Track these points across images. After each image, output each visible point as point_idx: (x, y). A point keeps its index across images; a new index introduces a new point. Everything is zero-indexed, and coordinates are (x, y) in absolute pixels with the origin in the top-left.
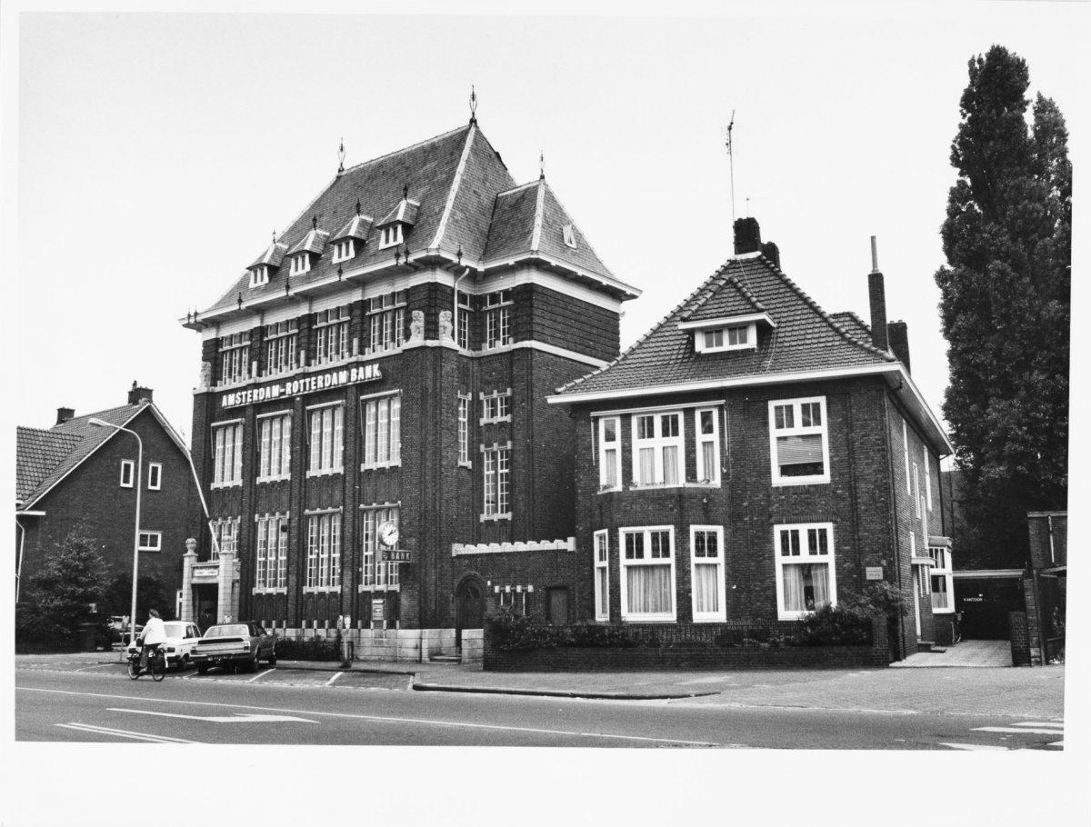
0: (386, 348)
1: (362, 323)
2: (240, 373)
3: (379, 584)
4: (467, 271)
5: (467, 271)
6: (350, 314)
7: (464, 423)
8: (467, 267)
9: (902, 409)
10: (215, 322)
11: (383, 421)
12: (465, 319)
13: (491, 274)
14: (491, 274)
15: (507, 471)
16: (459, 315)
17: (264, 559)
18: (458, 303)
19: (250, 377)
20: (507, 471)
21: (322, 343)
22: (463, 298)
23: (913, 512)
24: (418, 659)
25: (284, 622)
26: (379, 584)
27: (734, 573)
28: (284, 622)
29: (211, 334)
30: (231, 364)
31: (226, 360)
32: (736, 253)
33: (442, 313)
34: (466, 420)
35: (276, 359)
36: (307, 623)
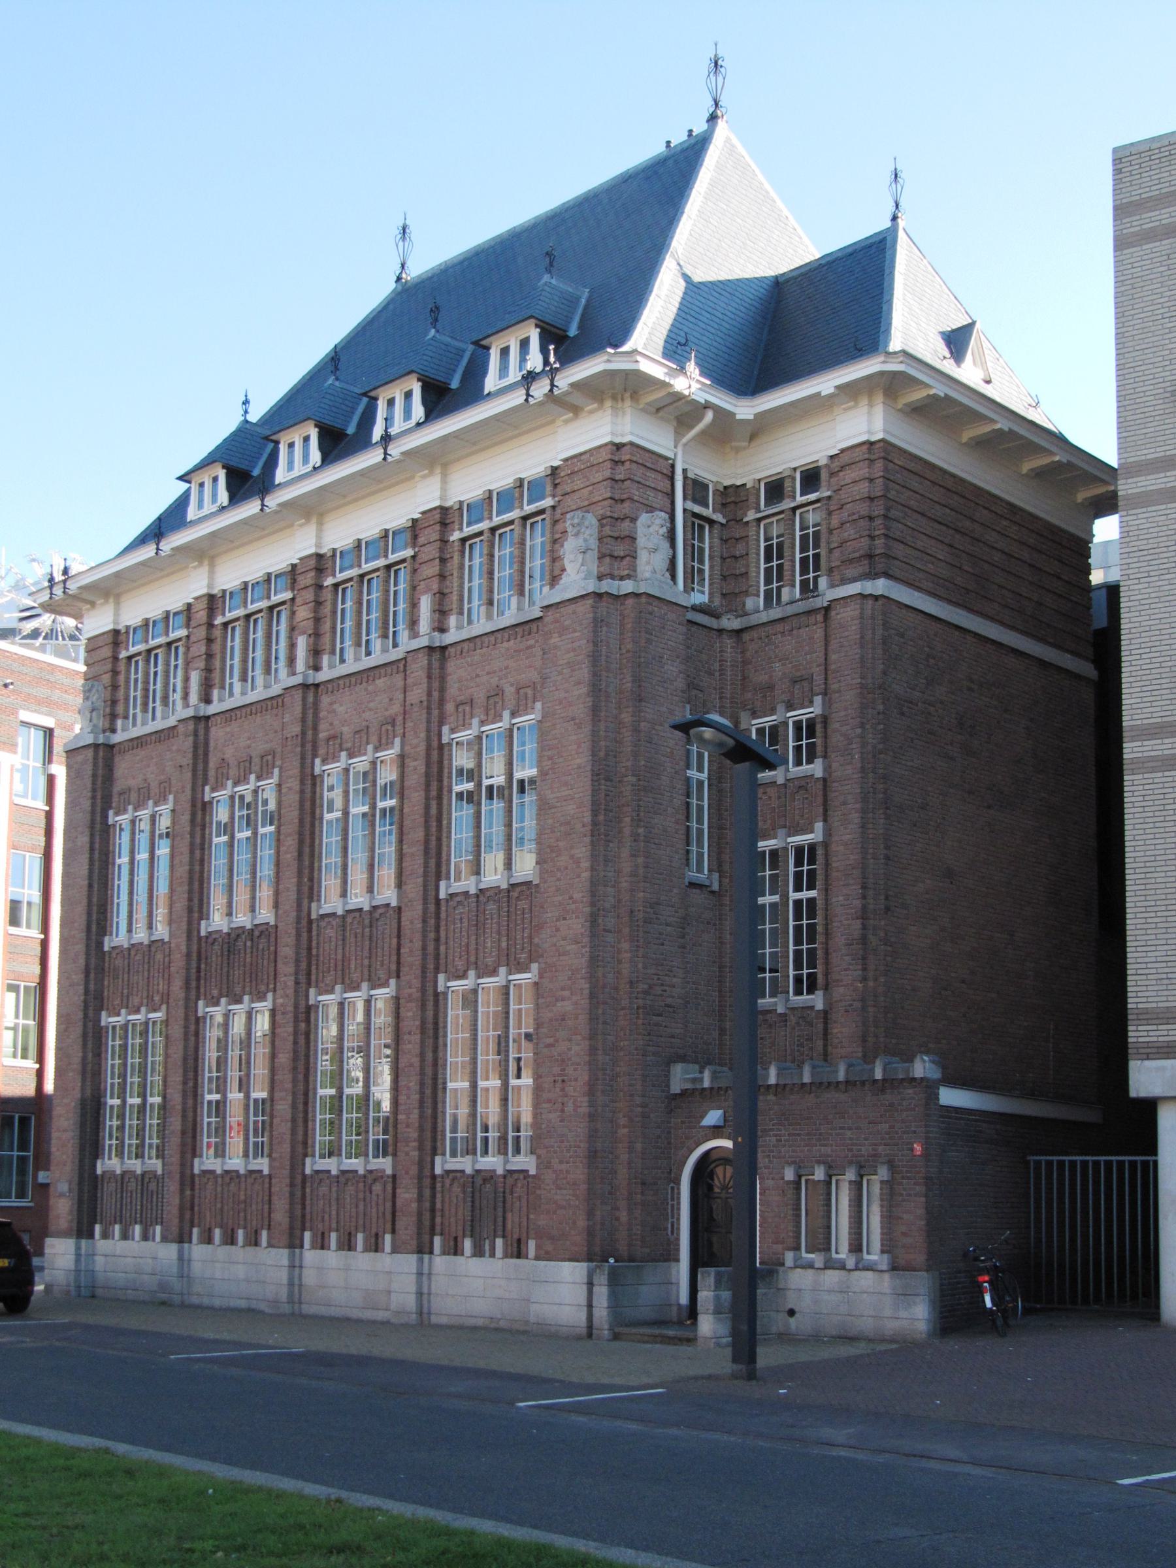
0: (368, 654)
1: (210, 641)
2: (165, 699)
3: (517, 1151)
4: (709, 416)
5: (709, 416)
6: (293, 585)
7: (700, 783)
8: (707, 406)
9: (300, 1138)
10: (109, 589)
11: (242, 857)
12: (701, 540)
13: (759, 429)
14: (759, 429)
15: (761, 900)
16: (689, 527)
17: (217, 1097)
18: (685, 498)
19: (293, 673)
20: (761, 900)
21: (140, 686)
22: (697, 489)
23: (717, 1298)
24: (584, 1331)
25: (264, 1234)
26: (485, 1152)
27: (755, 1329)
28: (264, 1234)
29: (99, 622)
30: (146, 682)
31: (137, 674)
32: (15, 753)
33: (644, 518)
34: (704, 776)
35: (359, 625)
36: (314, 1237)
